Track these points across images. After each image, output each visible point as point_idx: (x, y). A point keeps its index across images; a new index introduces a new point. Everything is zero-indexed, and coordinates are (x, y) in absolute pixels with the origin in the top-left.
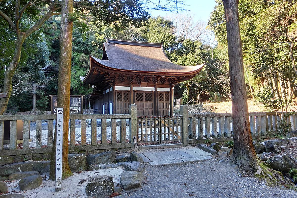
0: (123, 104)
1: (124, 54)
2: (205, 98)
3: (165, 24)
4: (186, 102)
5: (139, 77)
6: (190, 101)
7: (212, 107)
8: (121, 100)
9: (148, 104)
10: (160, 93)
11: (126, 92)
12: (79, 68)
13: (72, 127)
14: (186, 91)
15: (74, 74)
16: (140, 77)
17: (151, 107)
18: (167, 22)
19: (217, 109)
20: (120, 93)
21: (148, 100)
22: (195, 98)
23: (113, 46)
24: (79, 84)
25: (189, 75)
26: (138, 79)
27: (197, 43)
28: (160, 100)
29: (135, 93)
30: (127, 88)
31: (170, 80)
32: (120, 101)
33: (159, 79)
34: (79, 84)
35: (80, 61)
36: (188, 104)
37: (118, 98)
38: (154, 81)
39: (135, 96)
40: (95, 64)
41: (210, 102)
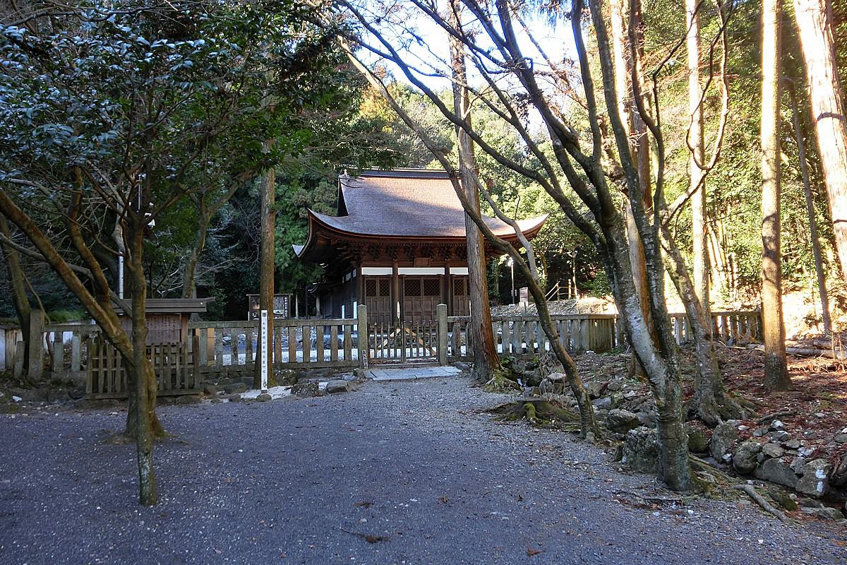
1: (380, 200)
12: (292, 220)
13: (277, 336)
15: (281, 236)
20: (372, 280)
30: (387, 271)
32: (372, 298)
33: (453, 250)
35: (292, 205)
37: (367, 292)
38: (442, 255)
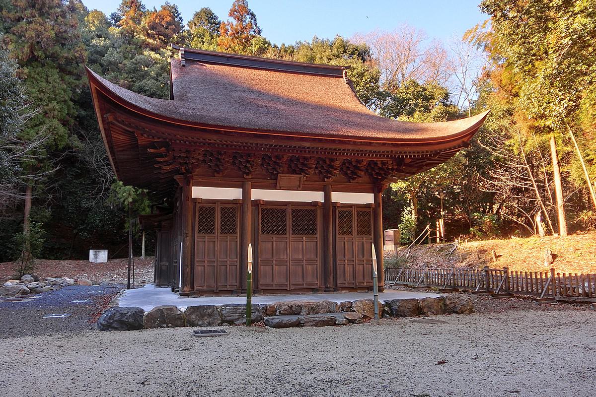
0: (218, 245)
2: (457, 229)
3: (353, 54)
4: (409, 238)
5: (270, 158)
6: (420, 236)
7: (483, 251)
8: (212, 231)
9: (301, 246)
10: (340, 209)
11: (231, 206)
14: (408, 208)
16: (276, 157)
17: (313, 256)
18: (356, 50)
19: (500, 256)
20: (208, 208)
21: (206, 231)
22: (433, 226)
23: (196, 68)
24: (138, 193)
25: (437, 148)
26: (268, 164)
27: (435, 90)
28: (342, 233)
29: (260, 208)
30: (233, 194)
31: (373, 169)
32: (206, 235)
33: (337, 164)
34: (138, 193)
36: (417, 242)
38: (320, 172)
39: (260, 218)
40: (110, 101)
41: (473, 237)
